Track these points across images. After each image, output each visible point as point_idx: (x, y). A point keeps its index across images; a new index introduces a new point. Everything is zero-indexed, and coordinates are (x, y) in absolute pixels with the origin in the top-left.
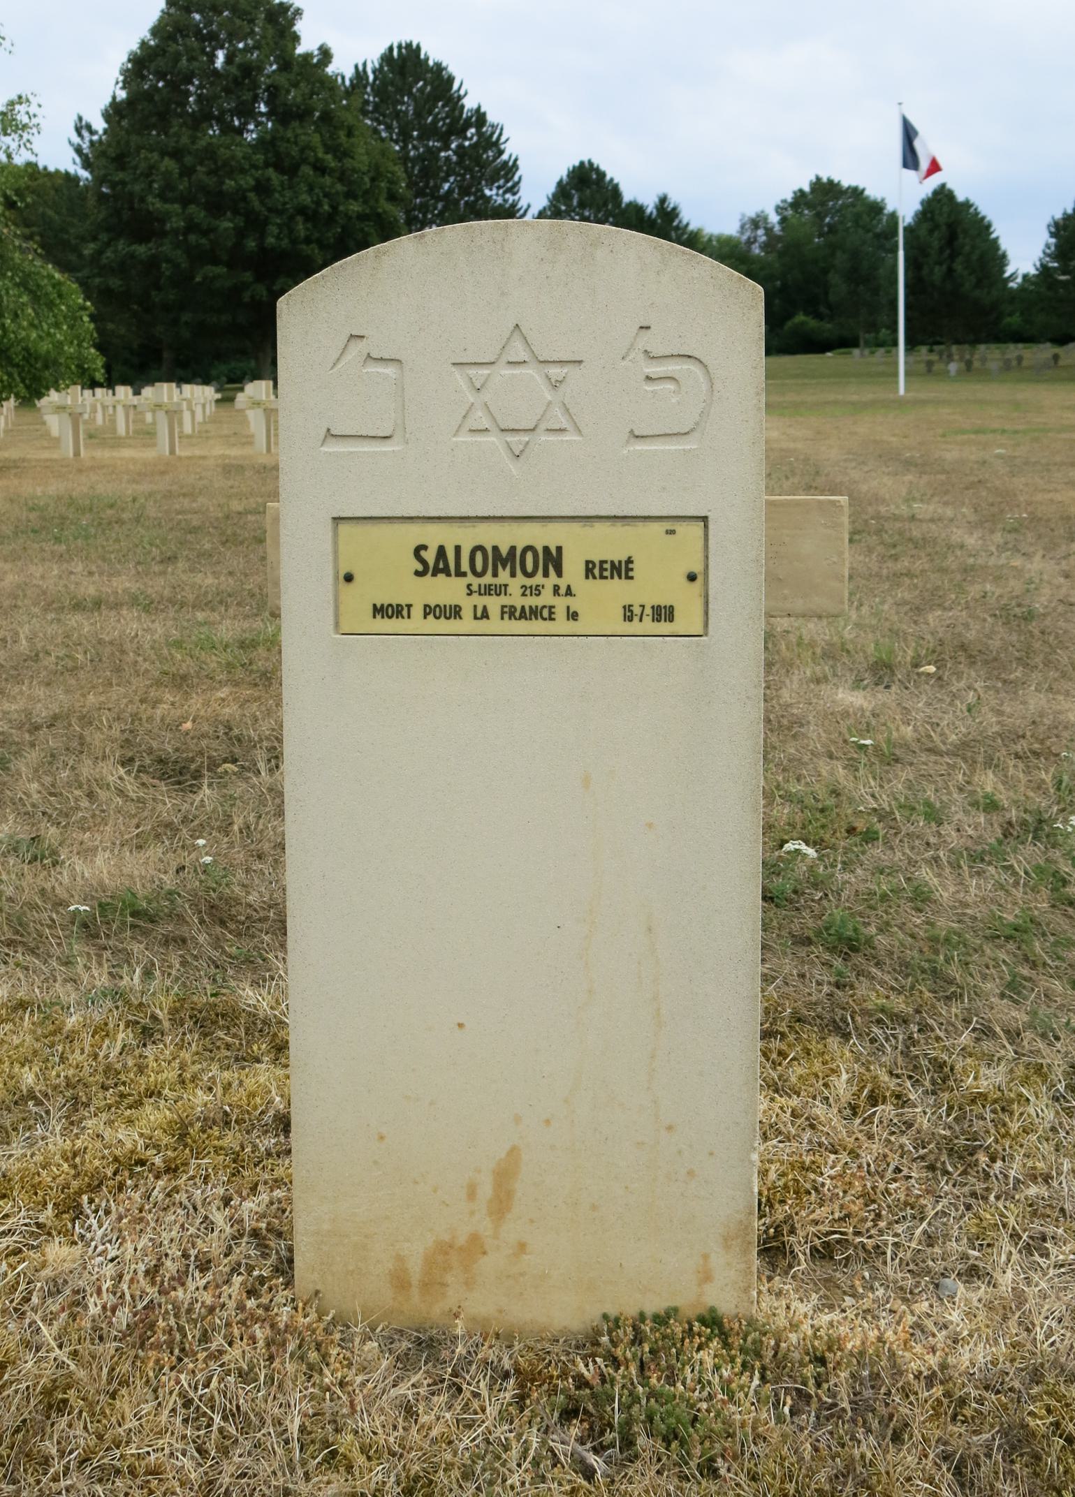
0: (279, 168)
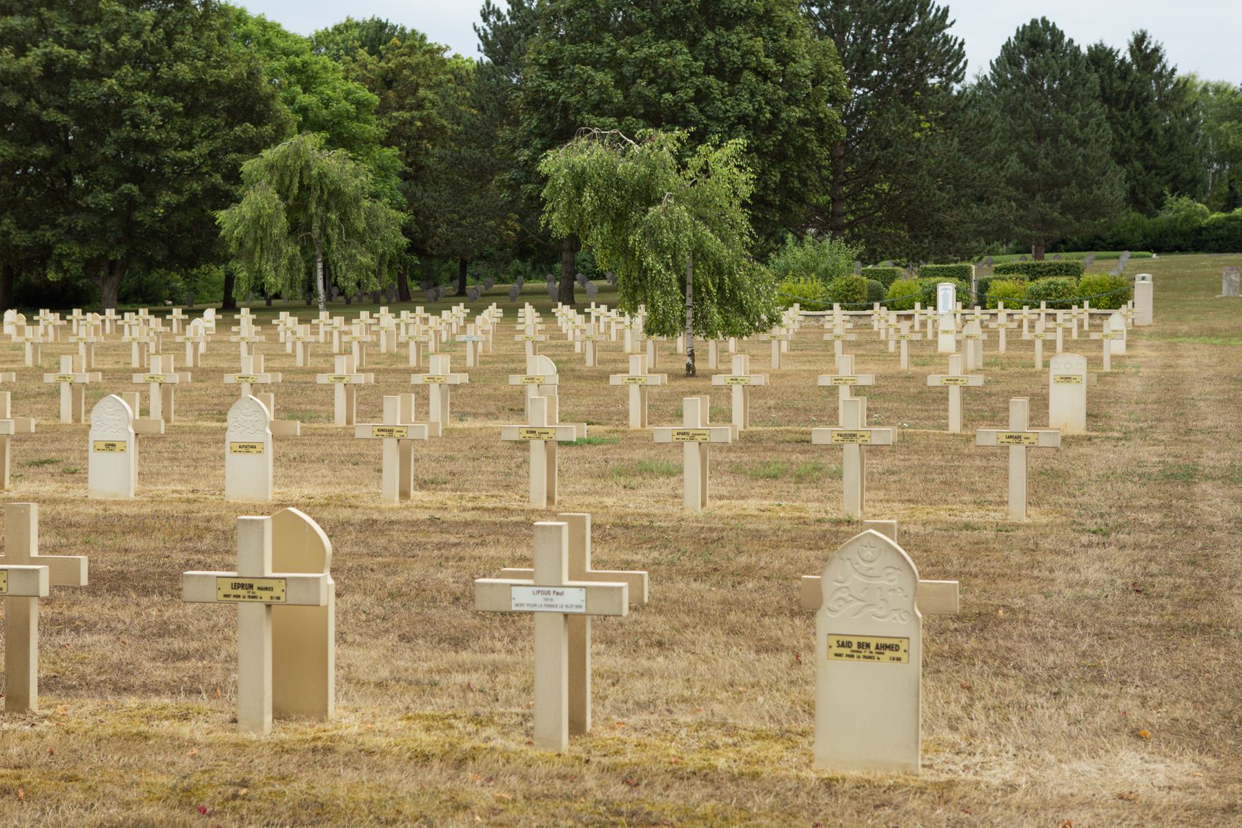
0: (720, 74)
